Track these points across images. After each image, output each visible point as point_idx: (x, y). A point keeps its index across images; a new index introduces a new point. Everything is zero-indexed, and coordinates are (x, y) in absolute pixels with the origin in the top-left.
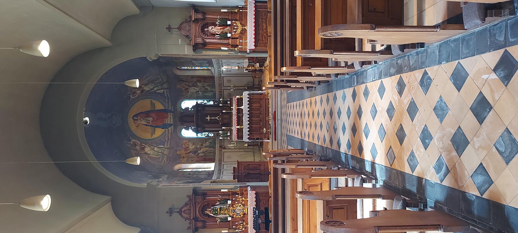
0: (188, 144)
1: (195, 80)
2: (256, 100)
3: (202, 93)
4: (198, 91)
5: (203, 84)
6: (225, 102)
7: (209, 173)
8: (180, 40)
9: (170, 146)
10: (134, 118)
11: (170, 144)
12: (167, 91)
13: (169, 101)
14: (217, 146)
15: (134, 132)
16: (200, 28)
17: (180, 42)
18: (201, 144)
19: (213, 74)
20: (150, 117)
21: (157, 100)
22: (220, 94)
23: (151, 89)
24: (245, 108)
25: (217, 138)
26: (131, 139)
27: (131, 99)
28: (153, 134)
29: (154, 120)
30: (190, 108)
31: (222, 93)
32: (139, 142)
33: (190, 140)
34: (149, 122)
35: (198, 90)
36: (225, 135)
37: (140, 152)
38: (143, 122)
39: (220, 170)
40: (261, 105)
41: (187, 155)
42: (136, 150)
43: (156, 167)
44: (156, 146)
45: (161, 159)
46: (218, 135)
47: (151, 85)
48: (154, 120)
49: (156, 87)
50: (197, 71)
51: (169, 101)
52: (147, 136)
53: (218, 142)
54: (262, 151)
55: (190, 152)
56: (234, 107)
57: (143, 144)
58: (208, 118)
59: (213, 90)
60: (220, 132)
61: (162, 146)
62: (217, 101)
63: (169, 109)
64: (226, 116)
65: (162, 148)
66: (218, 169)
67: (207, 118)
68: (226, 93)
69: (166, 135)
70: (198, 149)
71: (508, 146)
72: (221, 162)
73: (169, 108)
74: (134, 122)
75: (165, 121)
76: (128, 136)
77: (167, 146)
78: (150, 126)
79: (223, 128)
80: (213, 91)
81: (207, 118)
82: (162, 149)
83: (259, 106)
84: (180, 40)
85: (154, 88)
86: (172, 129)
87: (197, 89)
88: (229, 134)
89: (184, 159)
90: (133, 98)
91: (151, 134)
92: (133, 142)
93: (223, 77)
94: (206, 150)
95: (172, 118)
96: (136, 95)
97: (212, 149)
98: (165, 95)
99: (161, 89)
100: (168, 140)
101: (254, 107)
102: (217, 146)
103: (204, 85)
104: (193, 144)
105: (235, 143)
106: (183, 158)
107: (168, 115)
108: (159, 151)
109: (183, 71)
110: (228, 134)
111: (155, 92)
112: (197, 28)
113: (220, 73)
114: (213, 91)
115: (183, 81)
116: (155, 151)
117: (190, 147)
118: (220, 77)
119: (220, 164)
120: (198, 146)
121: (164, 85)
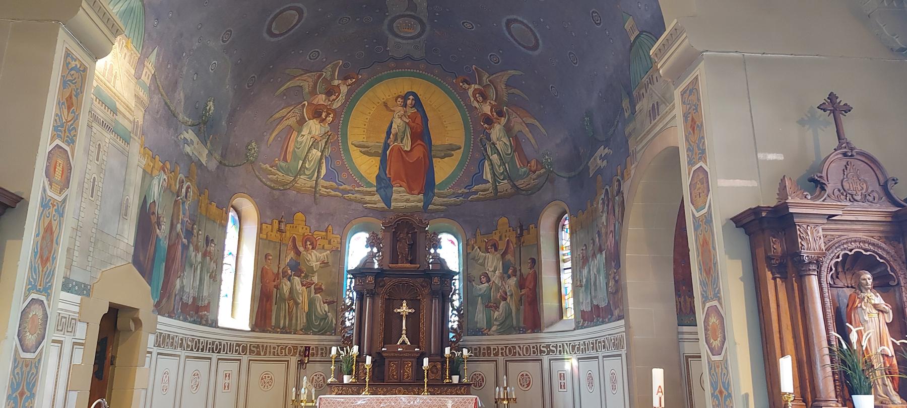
0: (326, 246)
1: (526, 270)
3: (482, 292)
4: (488, 280)
6: (456, 366)
7: (207, 308)
8: (780, 157)
9: (321, 195)
10: (411, 97)
14: (312, 340)
15: (369, 93)
16: (867, 246)
17: (771, 157)
19: (547, 327)
22: (482, 351)
23: (494, 144)
25: (340, 338)
26: (349, 81)
27: (466, 86)
28: (361, 149)
29: (404, 155)
30: (438, 251)
32: (340, 104)
33: (339, 253)
34: (399, 140)
35: (493, 279)
37: (306, 103)
38: (398, 124)
39: (216, 348)
42: (313, 93)
43: (253, 144)
44: (326, 154)
45: (283, 164)
46: (346, 342)
47: (508, 143)
48: (404, 155)
49: (501, 159)
50: (555, 276)
53: (325, 343)
54: (656, 81)
55: (298, 253)
57: (332, 115)
58: (404, 309)
59: (494, 328)
60: (356, 348)
61: (323, 171)
64: (408, 370)
65: (319, 172)
67: (404, 305)
68: (486, 369)
70: (306, 276)
72: (251, 352)
74: (399, 97)
76: (358, 74)
77: (323, 187)
78: (386, 143)
79: (369, 359)
80: (489, 325)
81: (404, 305)
84: (780, 157)
85: (499, 154)
87: (495, 278)
88: (345, 381)
90: (470, 92)
92: (338, 86)
93: (541, 360)
94: (300, 302)
95: (409, 204)
96: (478, 101)
97: (302, 320)
99: (494, 175)
100: (343, 190)
102: (312, 340)
103: (509, 298)
104: (323, 262)
107: (418, 194)
109: (552, 233)
110: (346, 379)
111: (485, 157)
112: (860, 235)
113: (553, 352)
115: (521, 235)
116: (309, 150)
118: (536, 353)
119: (244, 350)
120: (315, 279)
121: (506, 181)
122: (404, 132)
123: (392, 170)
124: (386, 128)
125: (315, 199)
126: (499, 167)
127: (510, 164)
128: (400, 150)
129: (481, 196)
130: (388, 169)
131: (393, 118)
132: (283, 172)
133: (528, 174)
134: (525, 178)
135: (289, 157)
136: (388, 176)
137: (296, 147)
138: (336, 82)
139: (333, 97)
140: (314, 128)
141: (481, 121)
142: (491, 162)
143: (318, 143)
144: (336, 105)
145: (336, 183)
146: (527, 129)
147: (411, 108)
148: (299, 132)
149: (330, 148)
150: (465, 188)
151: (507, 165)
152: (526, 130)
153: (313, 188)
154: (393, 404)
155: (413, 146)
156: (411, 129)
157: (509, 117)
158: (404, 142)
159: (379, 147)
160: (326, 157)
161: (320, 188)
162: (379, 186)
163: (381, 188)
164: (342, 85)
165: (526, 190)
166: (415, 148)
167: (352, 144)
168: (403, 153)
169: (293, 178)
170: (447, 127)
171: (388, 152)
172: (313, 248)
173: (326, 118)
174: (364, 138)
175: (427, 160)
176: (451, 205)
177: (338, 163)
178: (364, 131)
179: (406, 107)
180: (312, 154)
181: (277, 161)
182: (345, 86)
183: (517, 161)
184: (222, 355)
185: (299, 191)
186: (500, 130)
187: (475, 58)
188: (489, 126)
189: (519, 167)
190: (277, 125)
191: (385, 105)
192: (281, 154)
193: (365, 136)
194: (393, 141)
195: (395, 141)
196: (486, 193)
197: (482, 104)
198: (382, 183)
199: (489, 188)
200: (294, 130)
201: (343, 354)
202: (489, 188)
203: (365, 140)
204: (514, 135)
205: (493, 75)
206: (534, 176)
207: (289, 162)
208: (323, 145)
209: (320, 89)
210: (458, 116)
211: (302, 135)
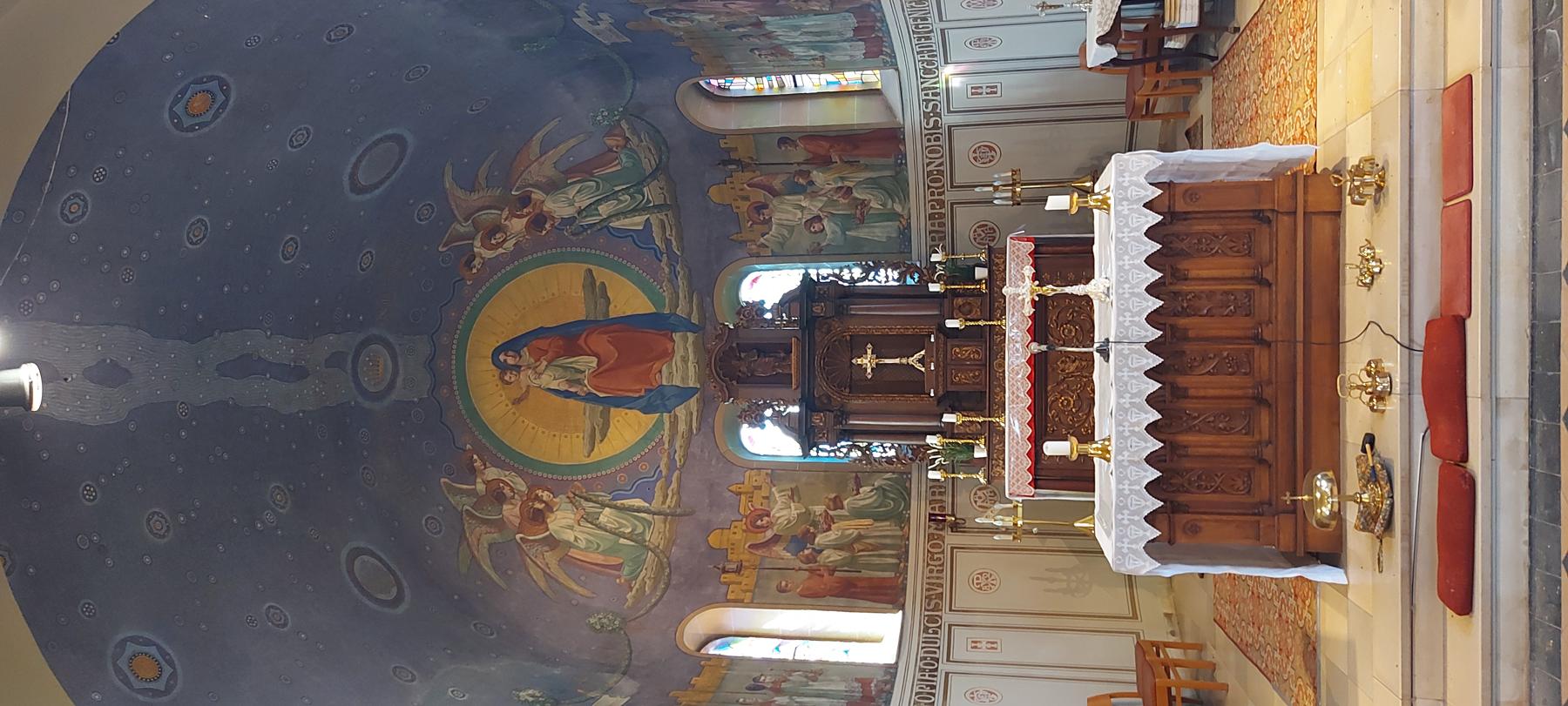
0: (764, 493)
2: (1215, 227)
3: (838, 229)
4: (818, 219)
5: (842, 179)
6: (960, 273)
9: (678, 504)
10: (502, 357)
14: (918, 511)
15: (497, 430)
18: (833, 496)
22: (936, 228)
23: (580, 212)
24: (1120, 297)
26: (478, 464)
27: (477, 262)
28: (598, 437)
30: (768, 306)
31: (942, 225)
32: (519, 480)
33: (776, 471)
35: (816, 212)
36: (960, 459)
37: (518, 536)
38: (551, 379)
39: (929, 665)
40: (1263, 265)
41: (759, 552)
42: (500, 525)
43: (592, 621)
44: (607, 498)
45: (626, 570)
47: (578, 187)
48: (606, 366)
49: (606, 199)
52: (568, 449)
53: (923, 489)
55: (776, 539)
56: (1021, 289)
57: (540, 493)
58: (867, 361)
59: (898, 208)
62: (919, 270)
64: (967, 352)
65: (639, 510)
66: (921, 654)
68: (966, 221)
69: (661, 442)
70: (815, 524)
71: (1012, 327)
72: (937, 608)
74: (502, 379)
75: (660, 372)
77: (664, 503)
79: (948, 418)
82: (636, 518)
83: (1249, 273)
85: (598, 202)
86: (692, 414)
87: (814, 206)
88: (984, 454)
89: (739, 579)
91: (587, 441)
92: (487, 483)
93: (950, 127)
94: (856, 532)
95: (691, 357)
96: (505, 241)
97: (887, 528)
99: (635, 211)
101: (1197, 288)
103: (847, 183)
104: (792, 498)
105: (1020, 510)
106: (738, 571)
108: (622, 525)
110: (981, 453)
113: (935, 106)
114: (894, 216)
115: (738, 162)
117: (777, 507)
118: (938, 135)
119: (932, 619)
122: (565, 368)
124: (559, 400)
126: (620, 202)
129: (673, 232)
130: (631, 394)
131: (540, 387)
134: (639, 157)
135: (613, 561)
137: (597, 549)
138: (481, 487)
139: (507, 491)
140: (562, 522)
141: (539, 233)
143: (588, 514)
144: (521, 486)
145: (657, 480)
148: (569, 545)
151: (617, 189)
157: (531, 186)
158: (582, 368)
163: (665, 405)
167: (589, 456)
168: (601, 370)
169: (650, 553)
170: (553, 294)
171: (602, 395)
172: (768, 515)
173: (544, 502)
174: (578, 437)
175: (612, 328)
176: (690, 285)
179: (521, 367)
183: (607, 171)
184: (942, 655)
185: (671, 542)
187: (426, 248)
189: (619, 168)
190: (557, 581)
191: (517, 402)
195: (581, 384)
197: (508, 234)
200: (566, 554)
201: (940, 459)
203: (581, 435)
204: (563, 175)
207: (622, 561)
208: (591, 504)
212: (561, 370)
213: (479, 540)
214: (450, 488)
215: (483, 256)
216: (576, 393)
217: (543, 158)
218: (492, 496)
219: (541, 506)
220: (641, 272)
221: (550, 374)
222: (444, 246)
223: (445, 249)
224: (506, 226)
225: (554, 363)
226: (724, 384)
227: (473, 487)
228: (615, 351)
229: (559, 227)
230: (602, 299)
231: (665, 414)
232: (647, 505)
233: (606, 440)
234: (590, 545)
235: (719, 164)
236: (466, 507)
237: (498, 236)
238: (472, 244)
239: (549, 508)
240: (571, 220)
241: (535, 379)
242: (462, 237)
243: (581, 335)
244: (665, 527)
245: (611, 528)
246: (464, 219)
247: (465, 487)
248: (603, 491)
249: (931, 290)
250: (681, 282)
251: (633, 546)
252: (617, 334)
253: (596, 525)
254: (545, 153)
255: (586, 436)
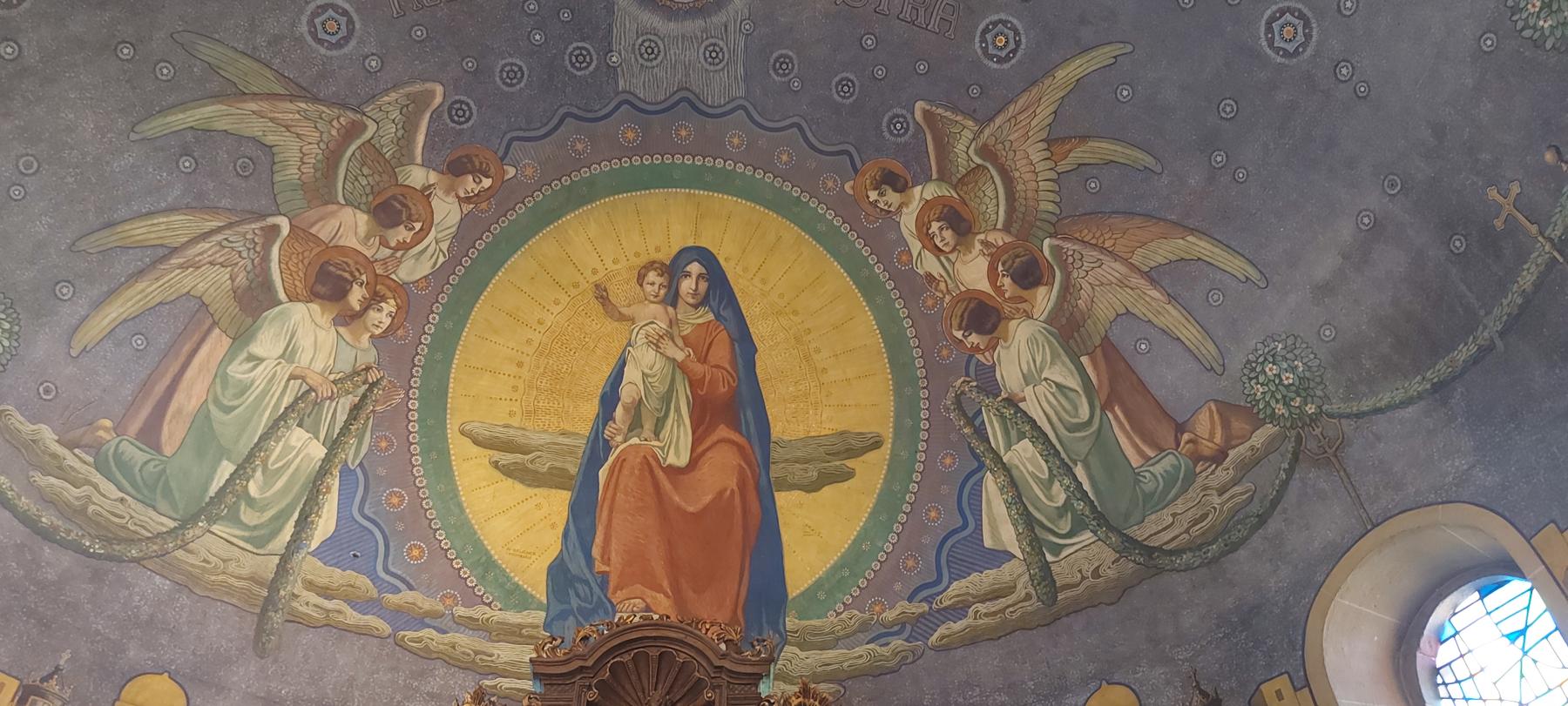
9: (295, 619)
10: (695, 268)
11: (329, 625)
12: (1011, 589)
13: (883, 634)
15: (543, 245)
20: (696, 443)
21: (887, 503)
23: (1012, 402)
26: (469, 185)
27: (893, 197)
28: (507, 458)
29: (666, 484)
32: (425, 268)
33: (213, 470)
34: (648, 426)
37: (284, 224)
42: (320, 190)
44: (352, 454)
45: (135, 454)
47: (1073, 382)
48: (666, 484)
51: (883, 634)
57: (389, 307)
61: (325, 524)
63: (789, 650)
65: (304, 523)
69: (472, 599)
73: (802, 646)
74: (650, 265)
77: (310, 585)
82: (281, 517)
85: (1039, 435)
91: (500, 432)
92: (426, 193)
96: (937, 251)
98: (957, 587)
99: (1027, 522)
108: (270, 476)
111: (983, 459)
121: (1087, 537)
122: (667, 398)
123: (614, 546)
124: (597, 381)
125: (260, 630)
126: (1047, 485)
127: (1093, 460)
128: (649, 464)
129: (986, 620)
130: (599, 539)
131: (629, 344)
132: (124, 482)
133: (1190, 478)
134: (1176, 497)
135: (172, 433)
136: (599, 567)
137: (217, 402)
138: (417, 176)
139: (401, 234)
141: (955, 323)
142: (1011, 477)
143: (317, 404)
144: (413, 269)
145: (374, 578)
146: (1155, 294)
147: (696, 306)
148: (241, 337)
149: (368, 434)
150: (910, 599)
151: (1079, 471)
152: (1151, 302)
153: (261, 584)
154: (1210, 658)
155: (700, 449)
156: (694, 384)
157: (1067, 276)
158: (665, 433)
159: (571, 451)
160: (346, 472)
161: (298, 589)
162: (557, 608)
163: (563, 616)
164: (440, 193)
165: (1195, 547)
166: (709, 454)
167: (462, 433)
168: (660, 474)
169: (172, 524)
170: (824, 370)
171: (603, 473)
173: (365, 309)
174: (512, 414)
175: (752, 496)
176: (857, 674)
177: (395, 500)
178: (515, 388)
179: (674, 305)
180: (288, 449)
181: (106, 429)
182: (451, 199)
183: (1123, 440)
185: (187, 582)
186: (1032, 341)
187: (922, 68)
188: (986, 338)
189: (1135, 461)
190: (140, 274)
191: (602, 295)
192: (132, 407)
193: (516, 408)
194: (625, 428)
195: (630, 429)
196: (1002, 602)
197: (953, 257)
198: (571, 592)
199: (1015, 581)
200: (215, 324)
202: (1015, 581)
203: (515, 422)
204: (1097, 341)
205: (991, 119)
206: (1222, 475)
207: (168, 451)
208: (342, 418)
209: (349, 186)
210: (865, 326)
211: (251, 358)
212: (663, 389)
213: (288, 128)
214: (418, 102)
215: (905, 210)
216: (612, 419)
217: (1141, 282)
218: (394, 197)
219: (356, 296)
220: (882, 556)
221: (657, 366)
222: (926, 113)
223: (918, 116)
224: (969, 248)
225: (679, 376)
226: (590, 663)
227: (419, 160)
228: (700, 506)
229: (974, 361)
230: (815, 474)
231: (543, 614)
232: (314, 545)
233: (497, 474)
234: (231, 391)
235: (1203, 694)
236: (372, 128)
237: (948, 234)
238: (930, 179)
239: (348, 318)
240: (988, 383)
241: (647, 336)
242: (944, 149)
243: (738, 430)
244: (239, 578)
245: (269, 451)
246: (985, 145)
247: (421, 139)
248: (370, 449)
249: (225, 462)
250: (862, 653)
251: (206, 490)
252: (739, 511)
253: (284, 417)
254: (1153, 282)
255: (512, 432)
